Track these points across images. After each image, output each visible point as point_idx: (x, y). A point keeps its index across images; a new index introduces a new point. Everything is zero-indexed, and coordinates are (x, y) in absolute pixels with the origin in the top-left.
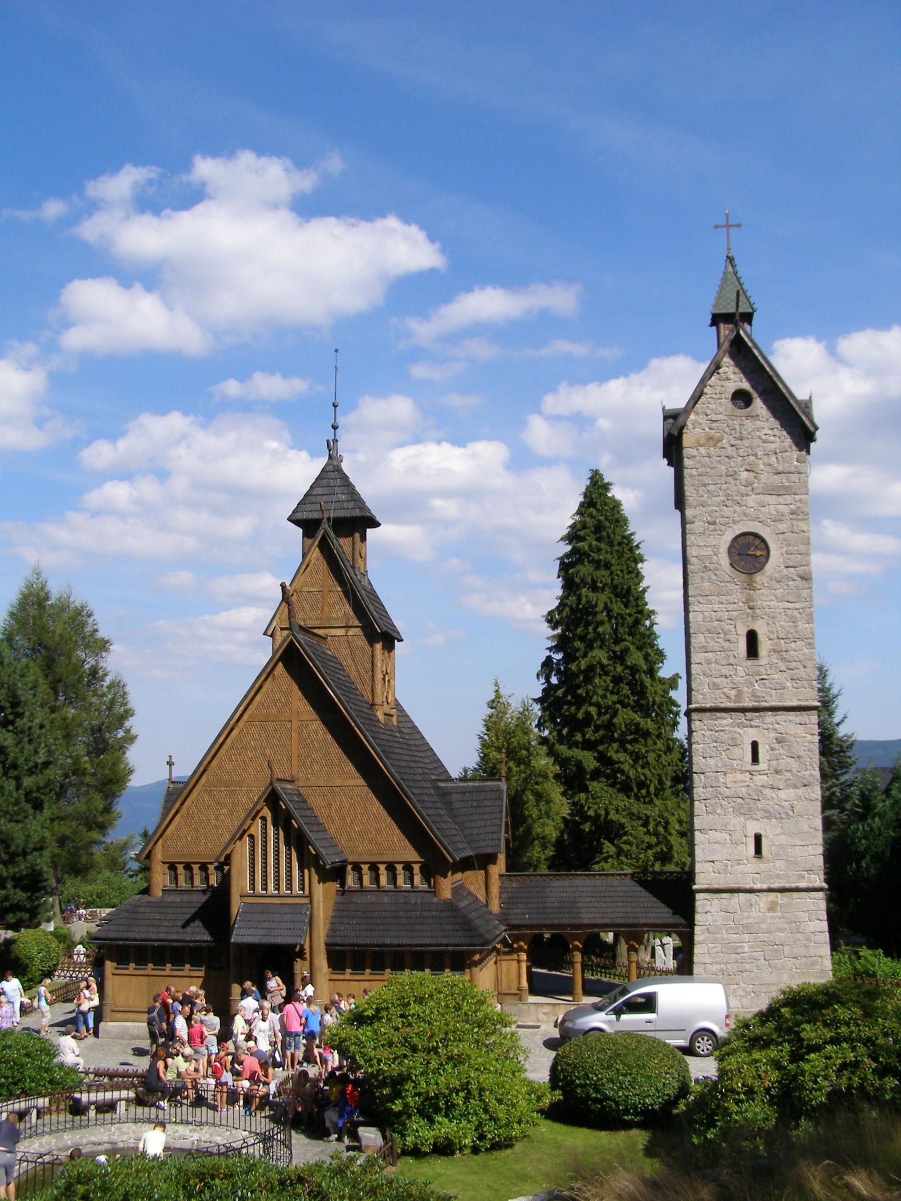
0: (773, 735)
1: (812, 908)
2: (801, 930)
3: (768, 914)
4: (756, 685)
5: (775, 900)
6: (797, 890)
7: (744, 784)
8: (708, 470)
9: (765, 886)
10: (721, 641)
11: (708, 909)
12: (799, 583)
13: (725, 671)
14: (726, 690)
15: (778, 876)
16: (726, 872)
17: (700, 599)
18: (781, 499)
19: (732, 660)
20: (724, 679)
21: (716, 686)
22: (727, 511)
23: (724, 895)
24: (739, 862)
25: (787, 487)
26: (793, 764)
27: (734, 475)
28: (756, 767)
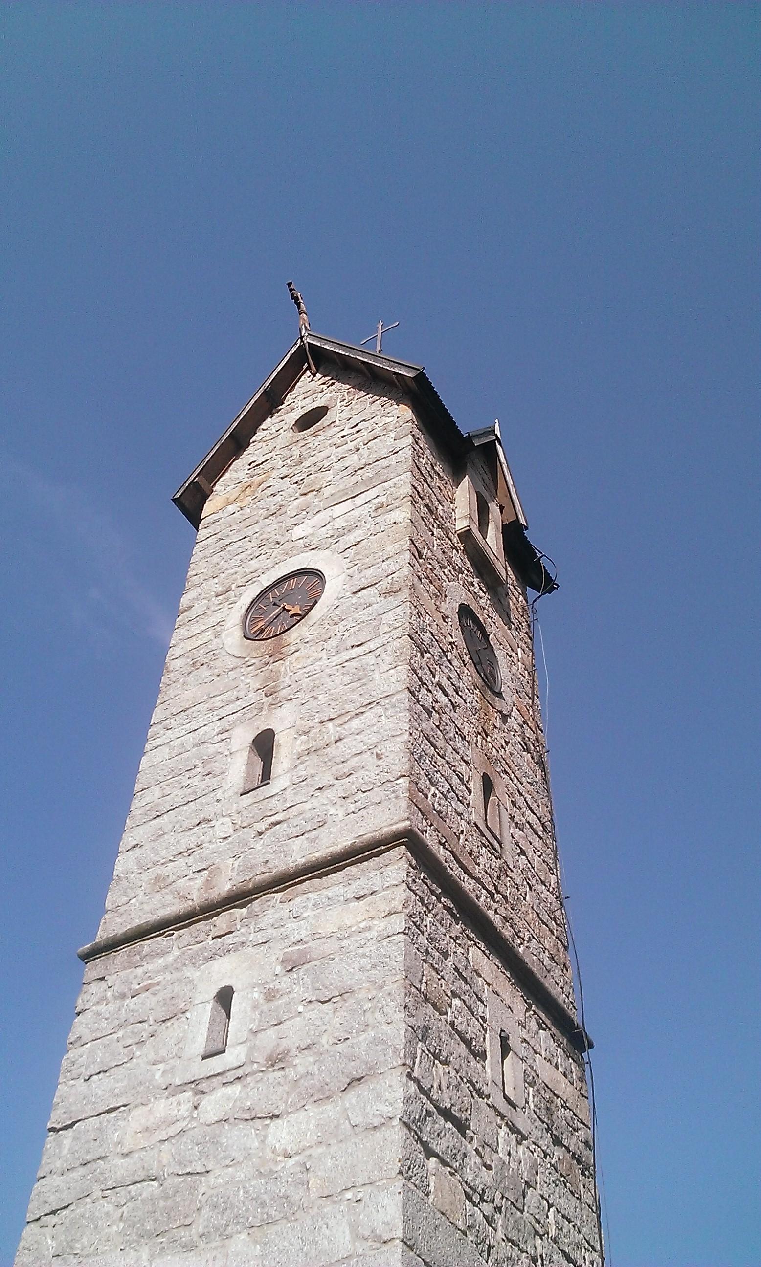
0: (277, 951)
7: (173, 1130)
13: (188, 840)
14: (181, 883)
18: (359, 500)
26: (332, 1020)
28: (216, 1064)
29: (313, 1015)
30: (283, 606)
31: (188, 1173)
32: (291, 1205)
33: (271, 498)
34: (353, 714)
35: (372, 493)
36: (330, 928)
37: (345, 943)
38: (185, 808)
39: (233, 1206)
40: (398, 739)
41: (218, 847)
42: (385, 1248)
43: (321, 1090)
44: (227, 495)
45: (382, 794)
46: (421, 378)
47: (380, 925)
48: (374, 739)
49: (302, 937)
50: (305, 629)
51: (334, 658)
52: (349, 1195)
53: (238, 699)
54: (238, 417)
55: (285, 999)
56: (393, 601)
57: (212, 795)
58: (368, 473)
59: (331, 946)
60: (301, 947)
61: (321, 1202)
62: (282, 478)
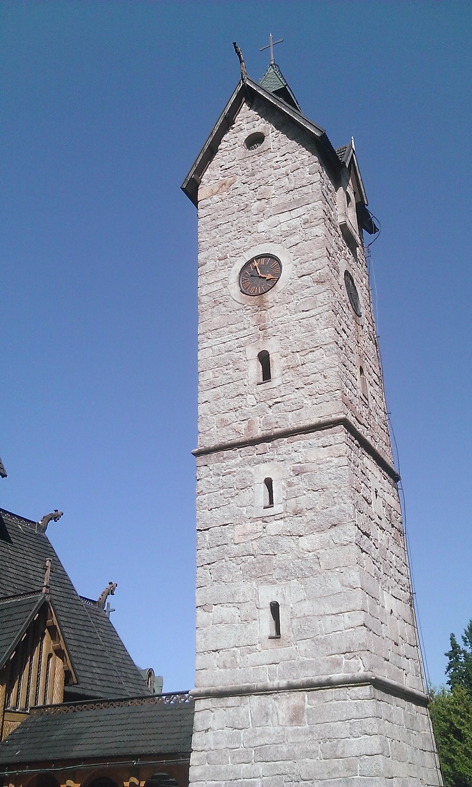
0: (289, 466)
1: (355, 714)
2: (339, 753)
3: (289, 729)
4: (270, 411)
5: (301, 703)
6: (330, 684)
7: (256, 536)
8: (220, 213)
9: (283, 683)
10: (231, 372)
11: (210, 724)
12: (315, 288)
13: (234, 403)
14: (234, 425)
15: (302, 665)
16: (234, 665)
17: (209, 334)
18: (294, 214)
19: (242, 390)
20: (232, 414)
21: (224, 423)
22: (237, 243)
23: (232, 701)
24: (250, 648)
25: (299, 200)
26: (319, 500)
27: (245, 209)
28: (270, 511)
29: (311, 495)
30: (260, 275)
31: (267, 555)
32: (314, 571)
33: (239, 197)
34: (309, 350)
35: (301, 211)
36: (313, 459)
37: (321, 466)
38: (228, 385)
39: (289, 569)
40: (334, 369)
41: (251, 410)
42: (354, 590)
43: (319, 527)
44: (211, 187)
45: (329, 397)
46: (324, 136)
47: (336, 461)
48: (321, 367)
49: (300, 461)
50: (275, 294)
51: (294, 316)
52: (338, 570)
53: (245, 329)
54: (212, 134)
55: (297, 487)
56: (322, 288)
57: (242, 381)
58: (296, 195)
59: (314, 467)
60: (301, 465)
61: (326, 571)
62: (244, 184)
